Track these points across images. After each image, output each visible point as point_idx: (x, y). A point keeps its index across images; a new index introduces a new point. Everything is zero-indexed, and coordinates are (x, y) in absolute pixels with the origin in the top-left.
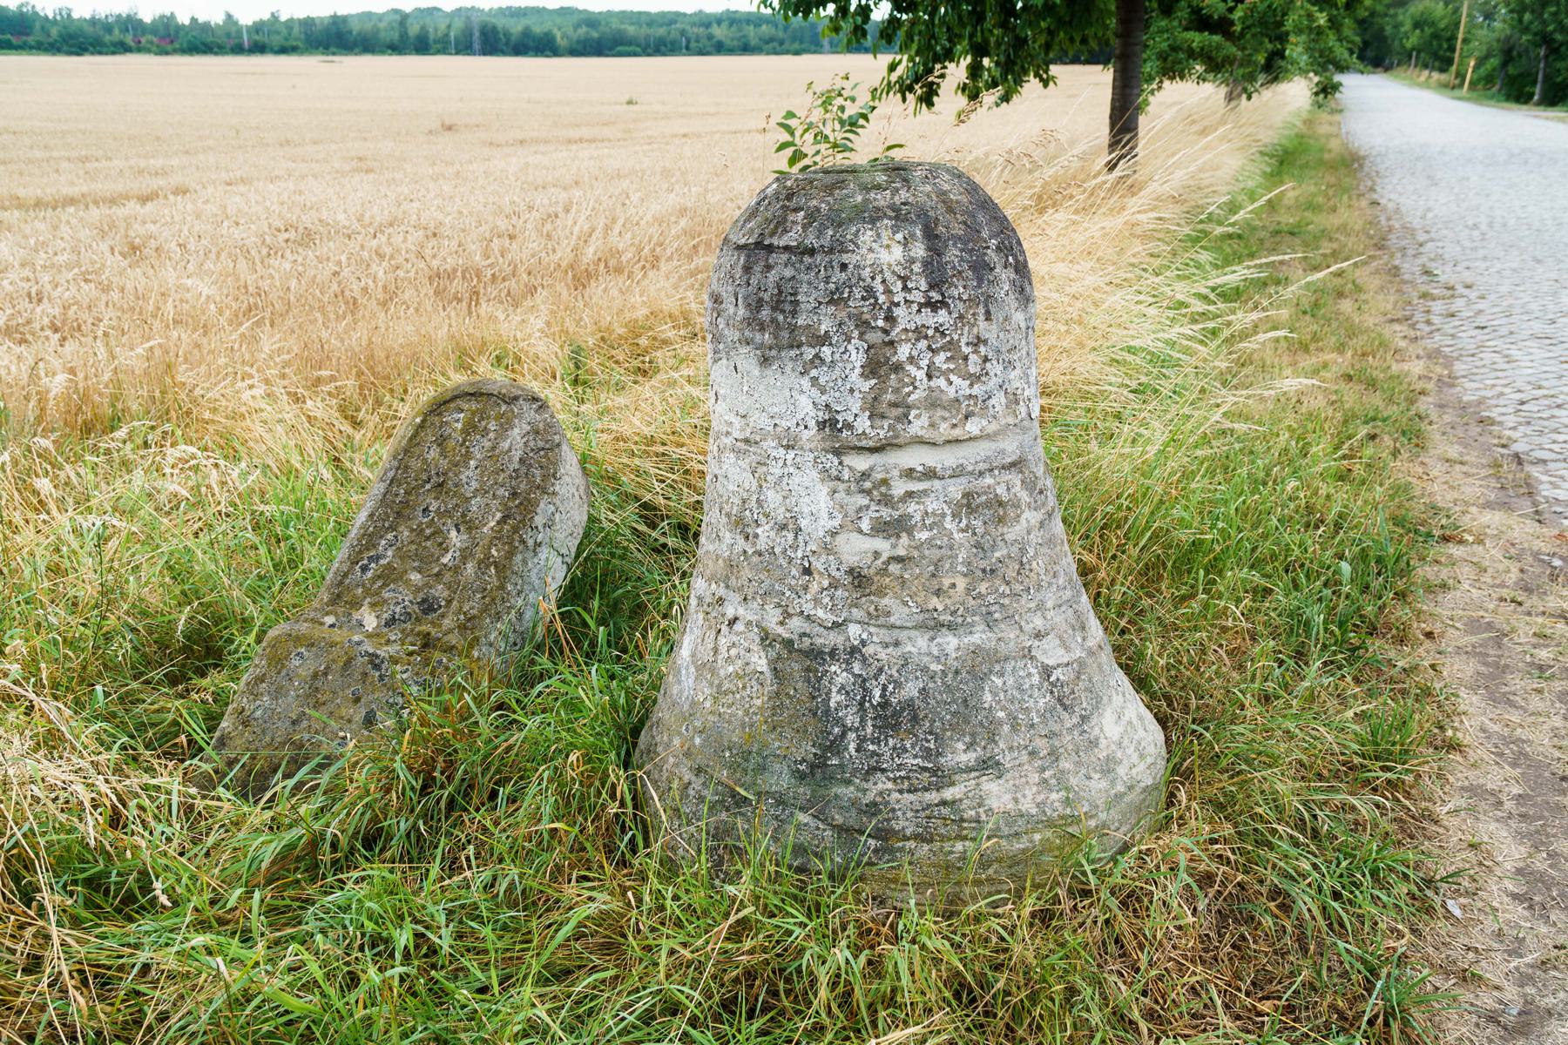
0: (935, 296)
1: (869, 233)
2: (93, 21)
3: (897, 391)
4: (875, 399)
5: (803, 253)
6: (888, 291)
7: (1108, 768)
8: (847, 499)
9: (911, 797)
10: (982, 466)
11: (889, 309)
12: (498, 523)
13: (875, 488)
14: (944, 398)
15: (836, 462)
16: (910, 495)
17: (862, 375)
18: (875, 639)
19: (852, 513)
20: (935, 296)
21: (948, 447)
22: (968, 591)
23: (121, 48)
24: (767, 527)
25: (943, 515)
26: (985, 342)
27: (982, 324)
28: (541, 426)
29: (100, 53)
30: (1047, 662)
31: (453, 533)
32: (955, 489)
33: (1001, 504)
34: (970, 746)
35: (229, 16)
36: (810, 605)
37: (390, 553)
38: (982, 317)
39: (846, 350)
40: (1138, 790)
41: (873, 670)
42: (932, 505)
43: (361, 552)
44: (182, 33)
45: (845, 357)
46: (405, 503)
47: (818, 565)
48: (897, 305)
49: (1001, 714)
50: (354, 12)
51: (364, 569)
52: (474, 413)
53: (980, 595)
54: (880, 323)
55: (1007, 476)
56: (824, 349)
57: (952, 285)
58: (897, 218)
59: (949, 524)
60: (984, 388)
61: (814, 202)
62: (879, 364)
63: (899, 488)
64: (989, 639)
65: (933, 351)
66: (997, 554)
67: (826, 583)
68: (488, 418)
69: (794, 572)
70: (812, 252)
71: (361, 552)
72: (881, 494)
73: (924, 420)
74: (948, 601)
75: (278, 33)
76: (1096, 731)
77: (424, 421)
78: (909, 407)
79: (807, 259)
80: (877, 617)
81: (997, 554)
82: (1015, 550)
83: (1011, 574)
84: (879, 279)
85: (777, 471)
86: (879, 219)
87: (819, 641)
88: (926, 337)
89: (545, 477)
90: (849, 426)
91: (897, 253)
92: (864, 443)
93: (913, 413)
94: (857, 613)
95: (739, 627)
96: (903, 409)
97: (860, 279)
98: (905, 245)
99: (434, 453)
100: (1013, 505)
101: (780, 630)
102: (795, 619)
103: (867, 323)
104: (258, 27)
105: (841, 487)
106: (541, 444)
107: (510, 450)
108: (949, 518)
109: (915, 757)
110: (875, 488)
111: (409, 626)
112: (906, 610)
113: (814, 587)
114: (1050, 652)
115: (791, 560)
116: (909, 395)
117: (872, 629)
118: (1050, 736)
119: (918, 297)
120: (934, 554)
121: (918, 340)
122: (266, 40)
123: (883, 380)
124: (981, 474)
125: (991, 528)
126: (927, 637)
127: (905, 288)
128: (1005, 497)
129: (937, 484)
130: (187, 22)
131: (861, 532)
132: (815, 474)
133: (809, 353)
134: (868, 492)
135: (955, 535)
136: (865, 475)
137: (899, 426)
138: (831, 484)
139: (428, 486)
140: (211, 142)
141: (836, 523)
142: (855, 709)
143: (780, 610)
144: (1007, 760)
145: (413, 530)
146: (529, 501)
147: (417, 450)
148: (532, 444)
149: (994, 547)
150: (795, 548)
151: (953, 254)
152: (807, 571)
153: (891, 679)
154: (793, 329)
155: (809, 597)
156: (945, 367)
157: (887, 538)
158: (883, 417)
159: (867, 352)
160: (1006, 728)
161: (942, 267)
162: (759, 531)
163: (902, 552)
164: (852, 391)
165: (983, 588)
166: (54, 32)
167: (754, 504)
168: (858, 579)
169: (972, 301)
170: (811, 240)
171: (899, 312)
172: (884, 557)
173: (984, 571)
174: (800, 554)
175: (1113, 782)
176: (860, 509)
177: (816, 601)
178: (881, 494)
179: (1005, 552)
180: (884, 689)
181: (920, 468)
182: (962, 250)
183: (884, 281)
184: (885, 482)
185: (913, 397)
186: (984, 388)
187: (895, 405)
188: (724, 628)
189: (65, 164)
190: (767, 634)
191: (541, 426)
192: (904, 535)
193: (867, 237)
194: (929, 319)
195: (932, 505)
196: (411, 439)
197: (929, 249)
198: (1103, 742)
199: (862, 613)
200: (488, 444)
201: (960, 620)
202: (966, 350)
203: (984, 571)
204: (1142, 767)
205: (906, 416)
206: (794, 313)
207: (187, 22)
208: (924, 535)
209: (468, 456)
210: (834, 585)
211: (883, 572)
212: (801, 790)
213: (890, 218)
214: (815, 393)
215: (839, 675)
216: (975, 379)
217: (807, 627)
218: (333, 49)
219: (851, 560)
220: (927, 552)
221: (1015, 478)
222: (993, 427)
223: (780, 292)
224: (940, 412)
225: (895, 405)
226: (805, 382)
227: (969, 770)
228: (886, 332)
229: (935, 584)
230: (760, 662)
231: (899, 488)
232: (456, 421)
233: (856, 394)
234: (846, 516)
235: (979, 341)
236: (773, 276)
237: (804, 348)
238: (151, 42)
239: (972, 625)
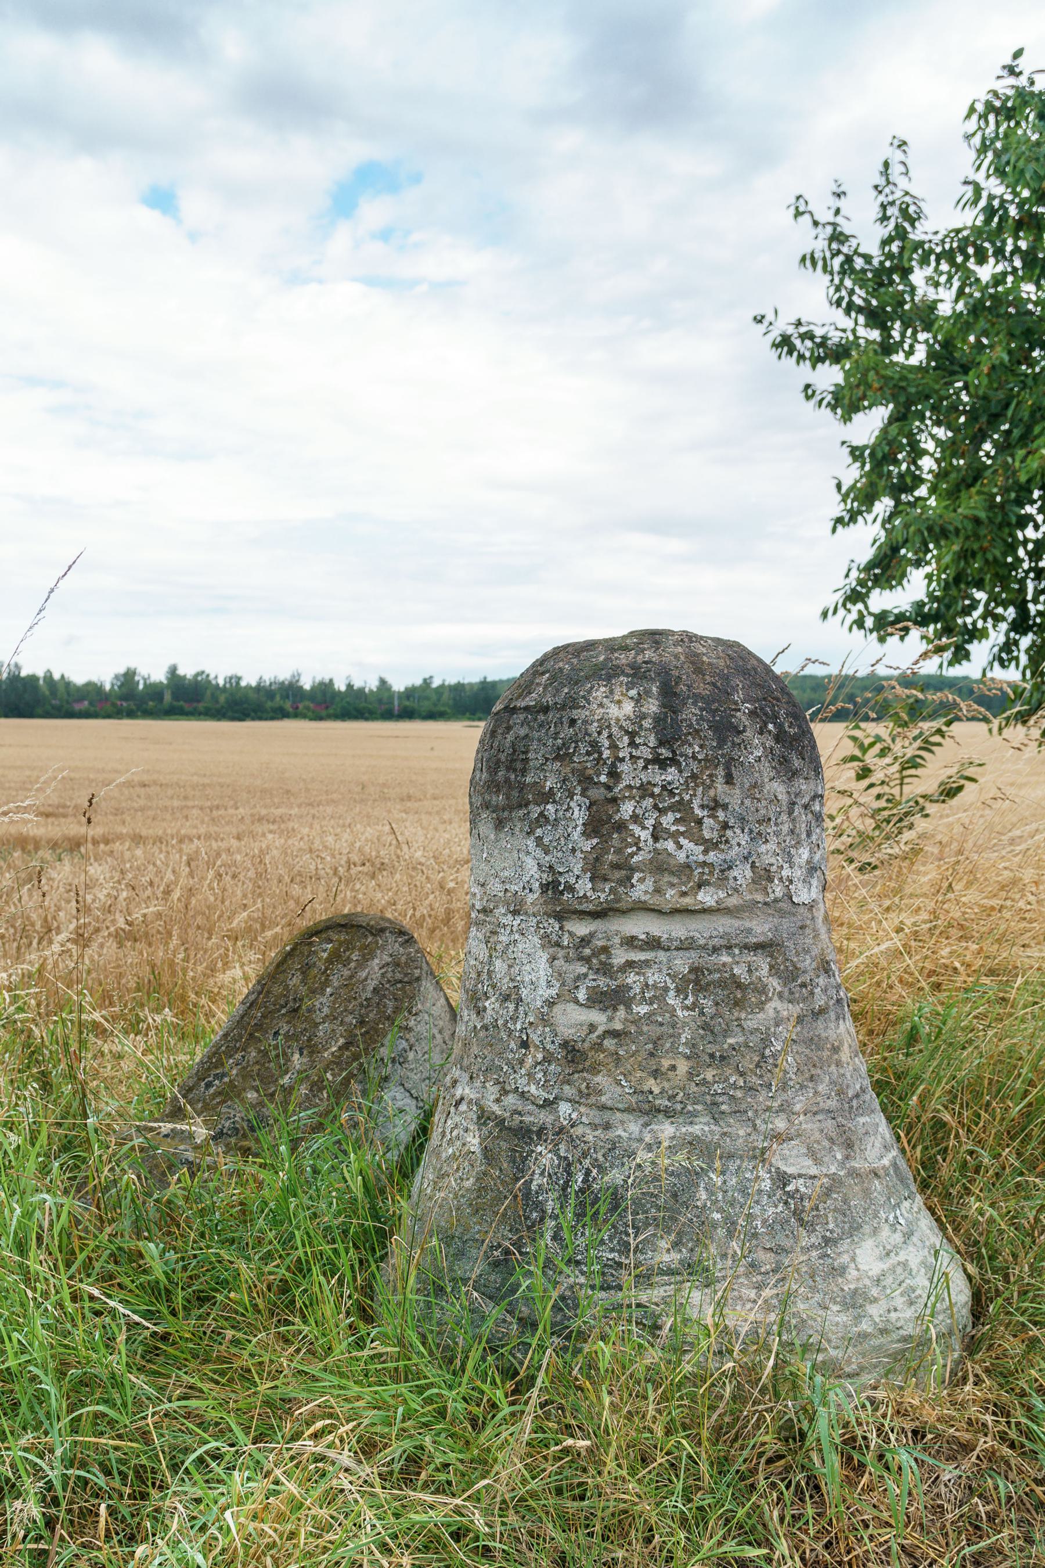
0: (665, 753)
1: (603, 689)
2: (258, 688)
3: (619, 851)
4: (597, 859)
5: (538, 712)
6: (614, 747)
7: (855, 1302)
8: (566, 967)
9: (603, 1294)
10: (717, 942)
11: (613, 765)
12: (340, 1048)
13: (593, 955)
14: (673, 862)
15: (557, 926)
16: (630, 964)
17: (583, 834)
18: (584, 1119)
19: (569, 981)
20: (665, 753)
21: (678, 917)
22: (690, 1075)
23: (280, 714)
24: (493, 999)
25: (666, 989)
26: (725, 807)
27: (720, 786)
28: (403, 959)
29: (260, 719)
30: (784, 1168)
31: (297, 1056)
32: (682, 963)
33: (739, 986)
34: (676, 1245)
35: (383, 682)
36: (524, 1081)
37: (234, 1072)
38: (721, 780)
39: (569, 808)
40: (895, 1336)
41: (578, 1153)
42: (653, 977)
43: (209, 1069)
44: (337, 699)
45: (568, 815)
46: (259, 1027)
47: (535, 1038)
48: (622, 760)
49: (717, 1216)
50: (505, 677)
51: (209, 1085)
52: (341, 944)
53: (704, 1082)
54: (603, 778)
55: (750, 957)
56: (549, 807)
57: (686, 742)
58: (634, 676)
59: (672, 1000)
60: (722, 856)
61: (561, 664)
62: (602, 822)
63: (620, 957)
64: (711, 1132)
65: (660, 810)
66: (731, 1041)
67: (540, 1057)
68: (354, 948)
69: (513, 1045)
70: (546, 709)
71: (209, 1069)
72: (601, 963)
73: (649, 884)
74: (666, 1085)
75: (427, 698)
76: (845, 1258)
77: (292, 950)
78: (633, 870)
79: (541, 717)
80: (586, 1096)
81: (731, 1041)
82: (754, 1040)
83: (748, 1062)
84: (605, 734)
85: (504, 939)
86: (617, 675)
87: (527, 1119)
88: (652, 795)
89: (397, 1010)
90: (570, 888)
91: (628, 708)
92: (584, 907)
93: (637, 876)
94: (568, 1091)
95: (463, 1107)
96: (626, 869)
97: (586, 734)
98: (637, 701)
99: (295, 981)
100: (755, 990)
101: (495, 1108)
102: (511, 1096)
103: (590, 778)
104: (410, 693)
105: (561, 953)
106: (398, 976)
107: (366, 979)
108: (672, 993)
109: (612, 1250)
110: (593, 955)
111: (233, 1140)
112: (619, 1089)
113: (529, 1061)
114: (792, 1160)
115: (511, 1032)
116: (632, 855)
117: (583, 1109)
118: (779, 1250)
119: (646, 753)
120: (654, 1031)
121: (643, 797)
122: (415, 705)
123: (605, 839)
124: (715, 950)
125: (725, 1010)
126: (641, 1122)
127: (632, 744)
128: (745, 978)
129: (662, 956)
130: (343, 688)
131: (576, 1001)
132: (536, 940)
133: (535, 811)
134: (587, 960)
135: (679, 1013)
136: (585, 941)
137: (621, 890)
138: (551, 950)
139: (283, 1011)
140: (335, 796)
141: (553, 992)
142: (556, 1195)
143: (497, 1088)
144: (719, 1268)
145: (260, 1051)
146: (376, 1031)
147: (281, 977)
148: (389, 975)
149: (726, 1033)
150: (514, 1019)
151: (691, 713)
152: (525, 1044)
153: (595, 1163)
154: (522, 787)
155: (523, 1071)
156: (673, 828)
157: (604, 1010)
158: (606, 880)
159: (589, 808)
160: (721, 1232)
161: (676, 724)
162: (487, 1004)
163: (618, 1026)
164: (574, 850)
165: (709, 1075)
166: (222, 699)
167: (485, 976)
168: (573, 1055)
169: (709, 762)
170: (549, 699)
171: (624, 768)
172: (600, 1030)
173: (712, 1056)
174: (519, 1027)
175: (858, 1319)
176: (578, 978)
177: (530, 1075)
178: (601, 963)
179: (741, 1039)
180: (588, 1173)
181: (643, 937)
182: (702, 709)
183: (610, 737)
184: (605, 950)
185: (635, 859)
186: (722, 856)
187: (616, 866)
188: (452, 1109)
189: (195, 812)
190: (483, 1111)
191: (403, 959)
192: (622, 1007)
193: (600, 693)
194: (657, 776)
195: (653, 977)
196: (278, 966)
197: (663, 705)
198: (852, 1273)
199: (574, 1091)
200: (346, 973)
201: (679, 1107)
202: (699, 812)
203: (712, 1056)
204: (909, 1313)
205: (629, 878)
206: (524, 771)
207: (343, 688)
208: (643, 1010)
209: (327, 983)
210: (548, 1059)
211: (598, 1046)
212: (493, 1277)
213: (627, 676)
214: (539, 853)
215: (545, 1157)
216: (709, 845)
217: (520, 1106)
218: (479, 715)
219: (567, 1032)
220: (645, 1029)
221: (763, 964)
222: (733, 901)
223: (515, 751)
224: (667, 878)
225: (616, 866)
226: (531, 843)
227: (671, 1272)
228: (609, 788)
229: (653, 1064)
230: (474, 1142)
231: (620, 957)
232: (324, 950)
233: (579, 854)
234: (563, 984)
235: (714, 806)
236: (510, 737)
237: (531, 806)
238: (308, 708)
239: (694, 1114)
